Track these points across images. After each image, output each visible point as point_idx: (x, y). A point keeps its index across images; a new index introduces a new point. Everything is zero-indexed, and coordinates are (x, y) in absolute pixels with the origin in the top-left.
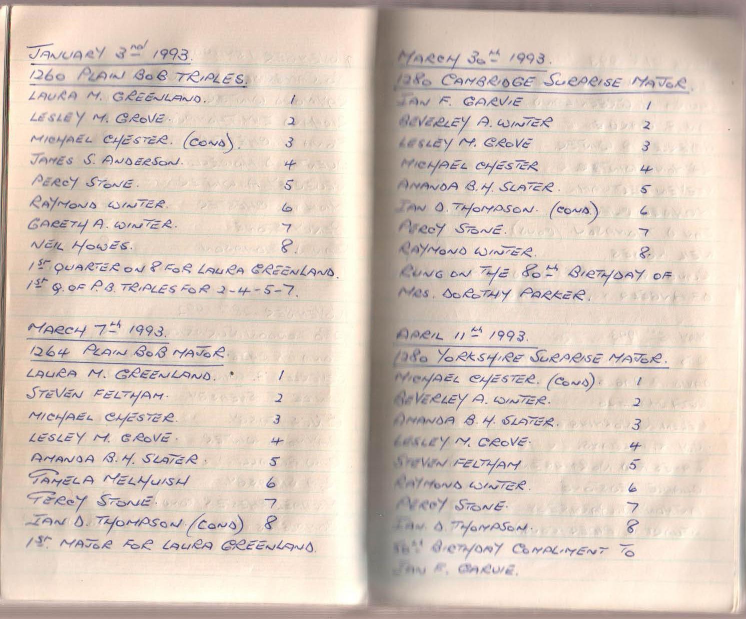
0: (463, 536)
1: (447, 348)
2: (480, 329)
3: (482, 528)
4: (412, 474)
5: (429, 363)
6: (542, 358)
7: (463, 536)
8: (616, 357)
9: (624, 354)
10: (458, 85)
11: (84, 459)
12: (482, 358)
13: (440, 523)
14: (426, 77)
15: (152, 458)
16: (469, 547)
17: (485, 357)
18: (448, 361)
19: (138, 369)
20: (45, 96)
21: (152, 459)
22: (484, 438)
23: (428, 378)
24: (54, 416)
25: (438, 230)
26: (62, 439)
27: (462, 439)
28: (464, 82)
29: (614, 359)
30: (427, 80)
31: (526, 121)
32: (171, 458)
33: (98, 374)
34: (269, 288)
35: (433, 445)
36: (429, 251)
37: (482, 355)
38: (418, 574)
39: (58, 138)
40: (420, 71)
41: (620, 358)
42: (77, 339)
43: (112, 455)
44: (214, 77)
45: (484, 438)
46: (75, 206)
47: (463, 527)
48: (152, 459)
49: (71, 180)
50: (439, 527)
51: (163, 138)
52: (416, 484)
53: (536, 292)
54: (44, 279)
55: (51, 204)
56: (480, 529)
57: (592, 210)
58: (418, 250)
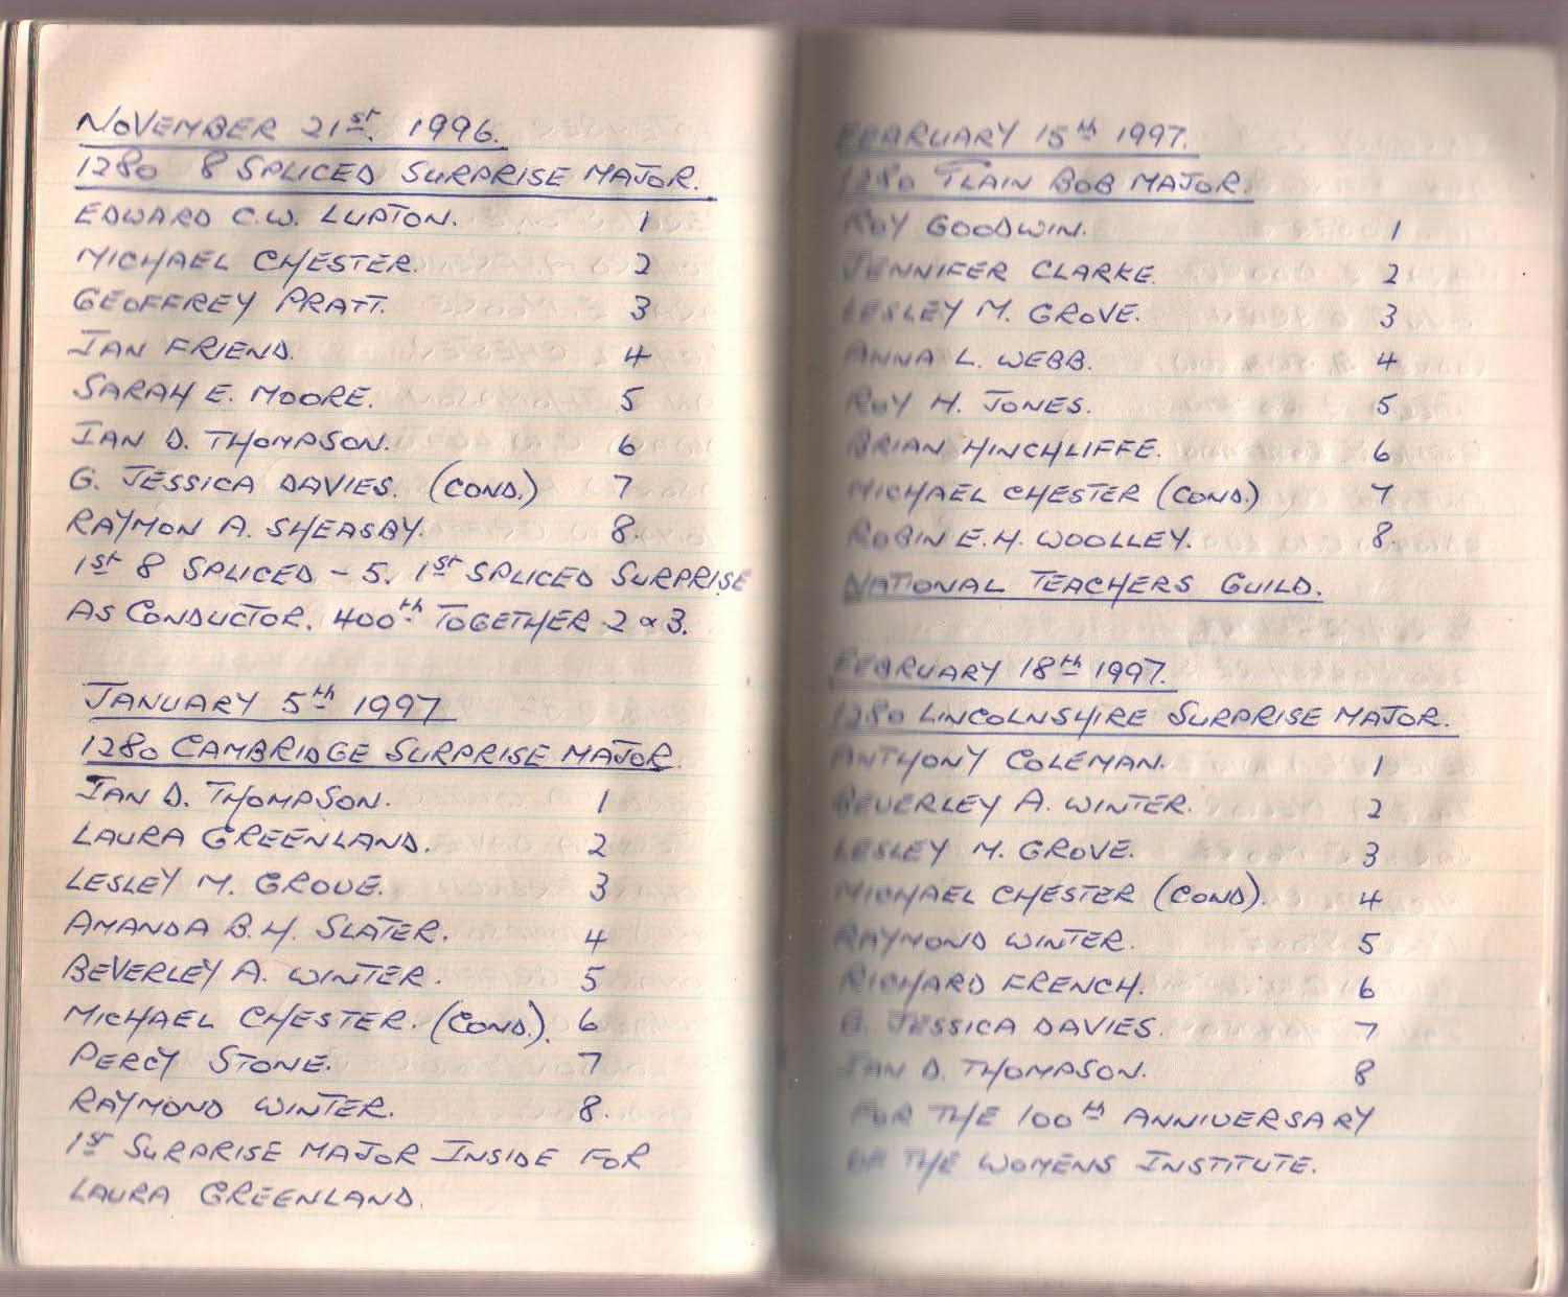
0: (988, 1089)
1: (988, 686)
2: (1101, 1107)
3: (1038, 1166)
4: (890, 917)
5: (920, 189)
6: (1193, 717)
7: (988, 1089)
8: (1348, 715)
9: (293, 807)
10: (206, 759)
11: (182, 930)
12: (191, 484)
13: (934, 1062)
14: (893, 706)
15: (339, 926)
16: (994, 1067)
17: (1070, 715)
18: (993, 724)
19: (448, 745)
20: (113, 217)
21: (339, 930)
22: (1016, 753)
23: (1029, 893)
24: (1108, 983)
25: (120, 1105)
26: (134, 886)
27: (210, 878)
28: (1150, 1120)
29: (1345, 719)
30: (922, 582)
31: (326, 1102)
32: (382, 926)
33: (999, 311)
34: (593, 974)
35: (948, 1172)
36: (927, 498)
37: (1064, 709)
38: (888, 1075)
39: (906, 488)
40: (883, 695)
41: (1355, 716)
42: (349, 717)
43: (244, 921)
44: (306, 296)
45: (1016, 753)
46: (1412, 721)
47: (986, 1070)
48: (339, 930)
49: (971, 752)
50: (932, 1070)
51: (1058, 845)
52: (882, 942)
53: (314, 295)
54: (112, 557)
55: (119, 523)
56: (1033, 1166)
57: (1250, 893)
58: (875, 940)
